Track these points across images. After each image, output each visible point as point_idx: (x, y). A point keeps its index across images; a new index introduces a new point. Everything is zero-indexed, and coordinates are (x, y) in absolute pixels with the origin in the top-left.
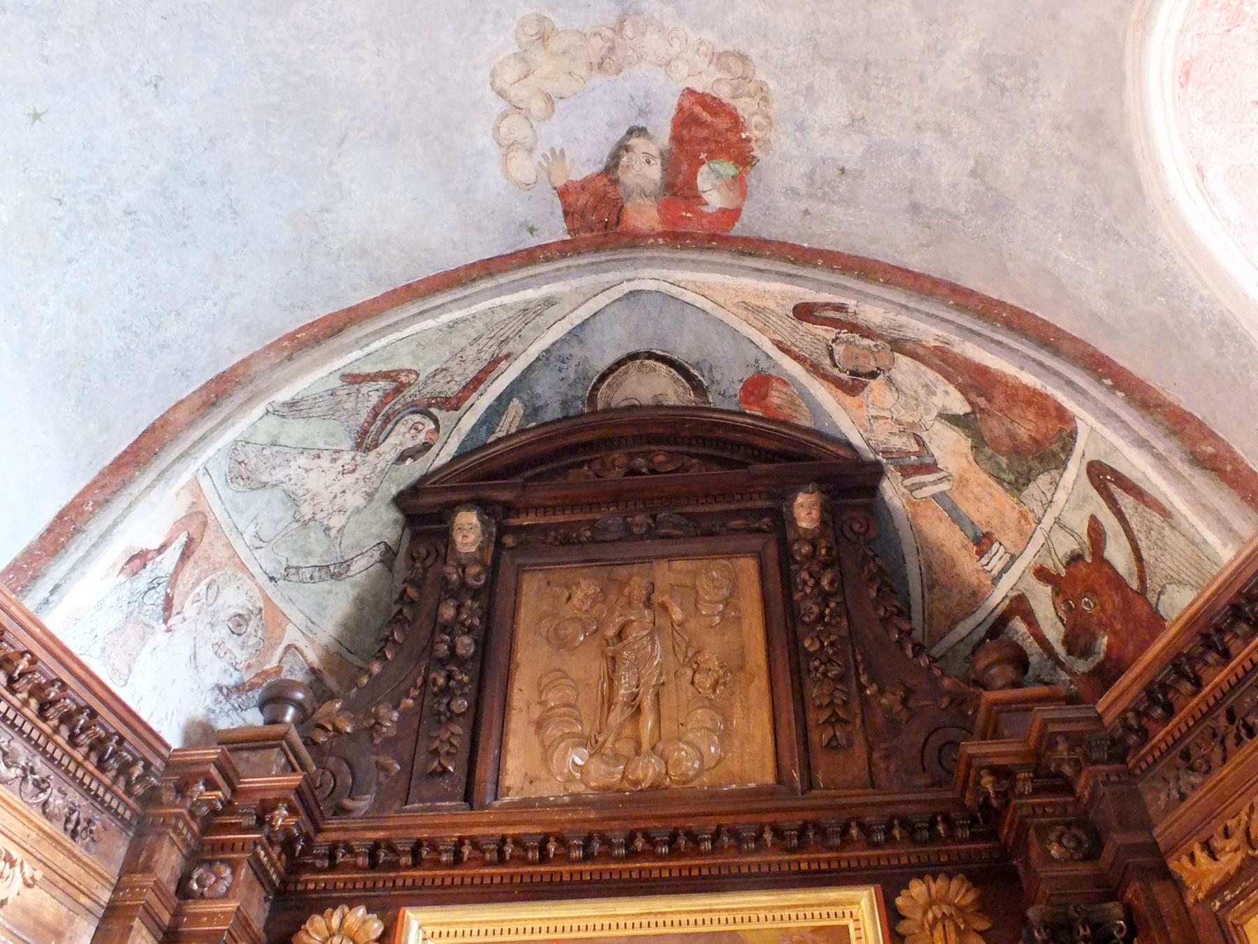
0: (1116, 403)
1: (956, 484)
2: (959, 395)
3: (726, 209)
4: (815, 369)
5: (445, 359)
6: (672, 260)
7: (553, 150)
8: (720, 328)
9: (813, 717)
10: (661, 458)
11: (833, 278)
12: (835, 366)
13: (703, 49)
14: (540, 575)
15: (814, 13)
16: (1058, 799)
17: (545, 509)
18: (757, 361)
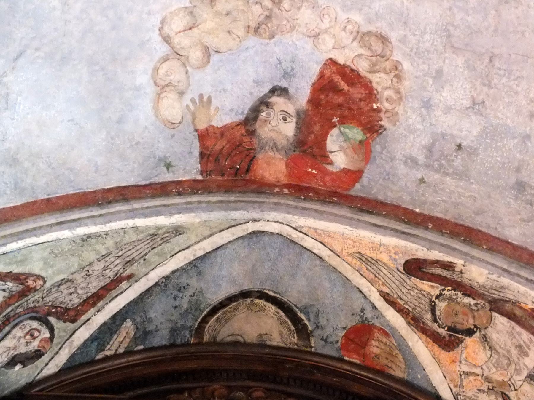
3: (349, 170)
4: (416, 322)
5: (73, 270)
6: (296, 207)
7: (201, 96)
8: (334, 276)
13: (350, 27)
15: (450, 9)
18: (362, 310)
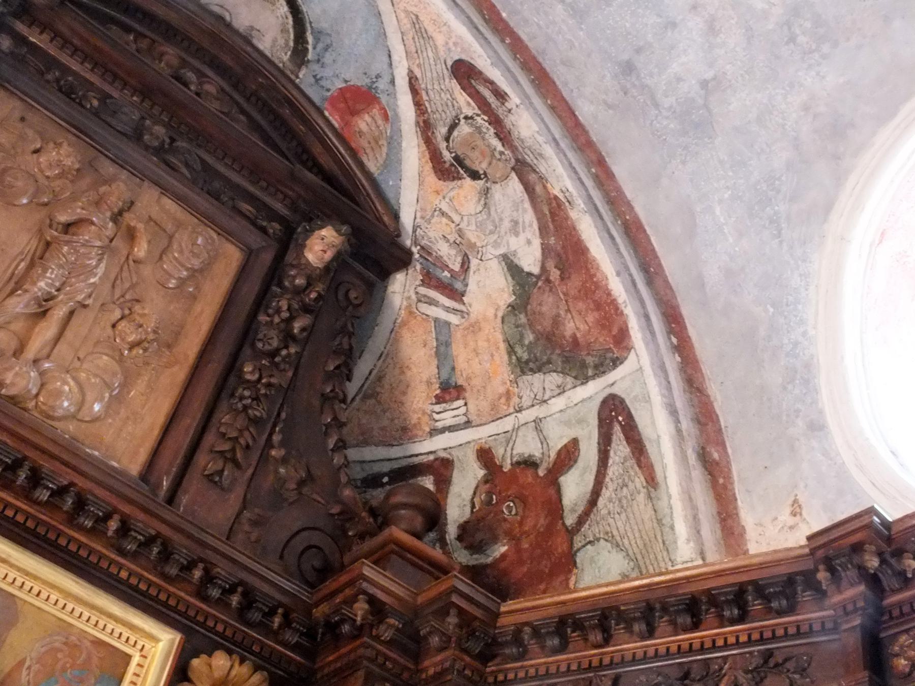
0: (672, 362)
1: (466, 324)
2: (538, 253)
4: (425, 127)
8: (373, 21)
9: (210, 438)
10: (210, 88)
11: (511, 63)
12: (447, 139)
14: (18, 103)
16: (402, 661)
17: (66, 43)
18: (378, 76)
